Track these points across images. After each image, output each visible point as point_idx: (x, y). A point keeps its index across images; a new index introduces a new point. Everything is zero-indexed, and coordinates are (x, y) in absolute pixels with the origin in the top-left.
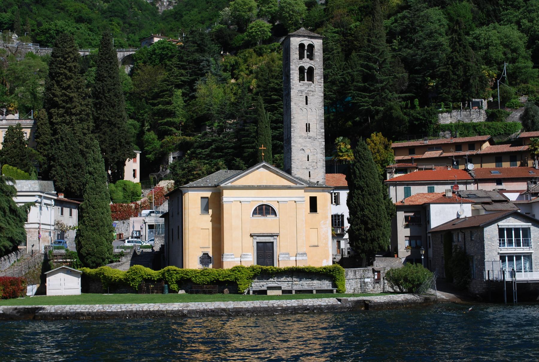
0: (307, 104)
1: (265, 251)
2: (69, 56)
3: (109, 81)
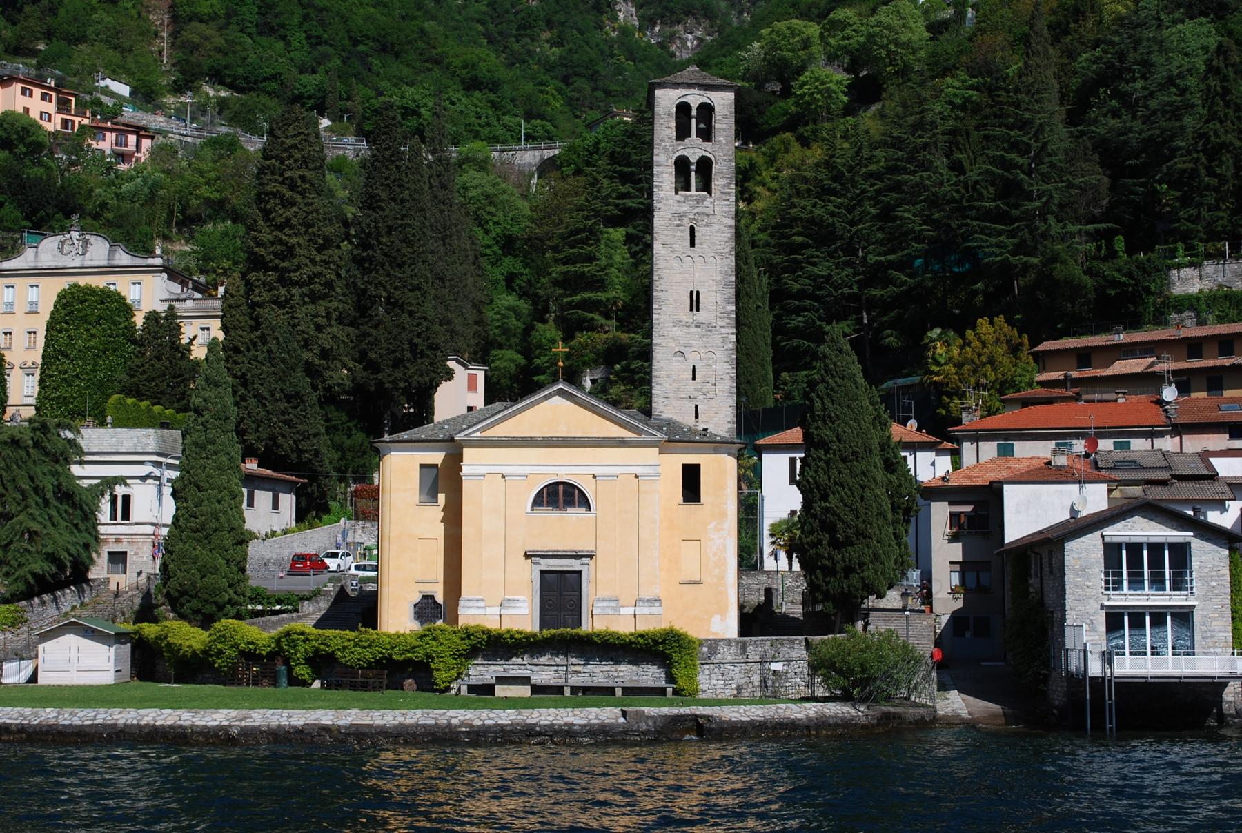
0: (692, 244)
1: (561, 590)
2: (290, 156)
3: (391, 209)
